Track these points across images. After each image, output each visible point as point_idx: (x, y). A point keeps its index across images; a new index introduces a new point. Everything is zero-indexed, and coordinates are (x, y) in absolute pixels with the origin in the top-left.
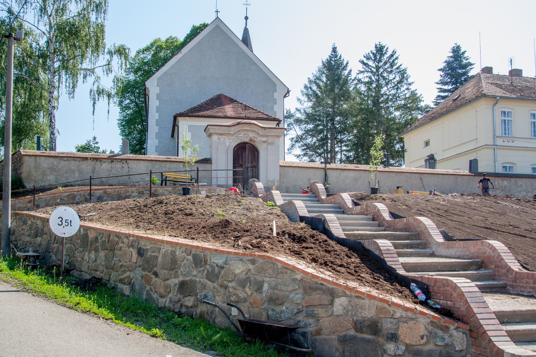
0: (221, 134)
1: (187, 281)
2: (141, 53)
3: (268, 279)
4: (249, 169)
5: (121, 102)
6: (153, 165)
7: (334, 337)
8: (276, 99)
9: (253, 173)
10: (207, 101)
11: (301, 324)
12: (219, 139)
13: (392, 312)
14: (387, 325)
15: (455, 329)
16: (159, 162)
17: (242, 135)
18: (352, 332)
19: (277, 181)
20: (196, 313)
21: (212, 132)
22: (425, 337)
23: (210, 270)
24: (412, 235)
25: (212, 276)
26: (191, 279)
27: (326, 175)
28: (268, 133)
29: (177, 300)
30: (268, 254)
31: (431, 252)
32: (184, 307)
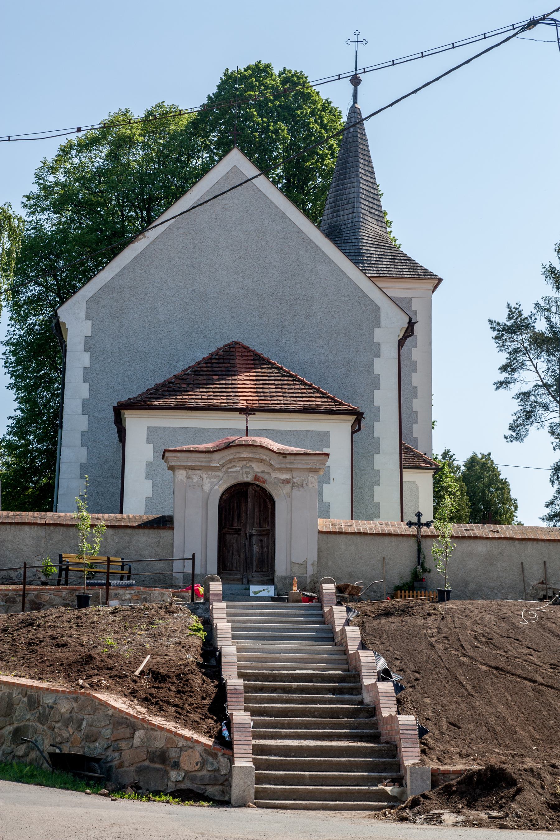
0: (193, 468)
1: (21, 727)
2: (74, 152)
3: (87, 716)
4: (255, 538)
5: (15, 291)
6: (49, 535)
7: (132, 768)
8: (379, 344)
9: (262, 547)
10: (198, 363)
11: (109, 759)
12: (188, 477)
13: (177, 742)
14: (173, 754)
15: (222, 755)
16: (62, 528)
17: (239, 469)
18: (147, 763)
19: (313, 564)
20: (26, 762)
21: (173, 464)
22: (199, 764)
23: (41, 712)
24: (350, 676)
25: (43, 719)
26: (25, 725)
27: (419, 551)
28: (291, 463)
29: (9, 751)
30: (88, 692)
31: (360, 699)
32: (16, 758)
